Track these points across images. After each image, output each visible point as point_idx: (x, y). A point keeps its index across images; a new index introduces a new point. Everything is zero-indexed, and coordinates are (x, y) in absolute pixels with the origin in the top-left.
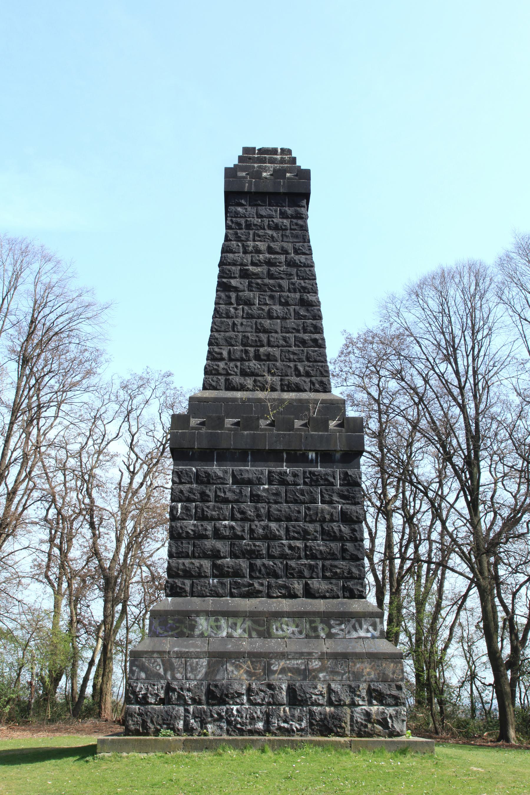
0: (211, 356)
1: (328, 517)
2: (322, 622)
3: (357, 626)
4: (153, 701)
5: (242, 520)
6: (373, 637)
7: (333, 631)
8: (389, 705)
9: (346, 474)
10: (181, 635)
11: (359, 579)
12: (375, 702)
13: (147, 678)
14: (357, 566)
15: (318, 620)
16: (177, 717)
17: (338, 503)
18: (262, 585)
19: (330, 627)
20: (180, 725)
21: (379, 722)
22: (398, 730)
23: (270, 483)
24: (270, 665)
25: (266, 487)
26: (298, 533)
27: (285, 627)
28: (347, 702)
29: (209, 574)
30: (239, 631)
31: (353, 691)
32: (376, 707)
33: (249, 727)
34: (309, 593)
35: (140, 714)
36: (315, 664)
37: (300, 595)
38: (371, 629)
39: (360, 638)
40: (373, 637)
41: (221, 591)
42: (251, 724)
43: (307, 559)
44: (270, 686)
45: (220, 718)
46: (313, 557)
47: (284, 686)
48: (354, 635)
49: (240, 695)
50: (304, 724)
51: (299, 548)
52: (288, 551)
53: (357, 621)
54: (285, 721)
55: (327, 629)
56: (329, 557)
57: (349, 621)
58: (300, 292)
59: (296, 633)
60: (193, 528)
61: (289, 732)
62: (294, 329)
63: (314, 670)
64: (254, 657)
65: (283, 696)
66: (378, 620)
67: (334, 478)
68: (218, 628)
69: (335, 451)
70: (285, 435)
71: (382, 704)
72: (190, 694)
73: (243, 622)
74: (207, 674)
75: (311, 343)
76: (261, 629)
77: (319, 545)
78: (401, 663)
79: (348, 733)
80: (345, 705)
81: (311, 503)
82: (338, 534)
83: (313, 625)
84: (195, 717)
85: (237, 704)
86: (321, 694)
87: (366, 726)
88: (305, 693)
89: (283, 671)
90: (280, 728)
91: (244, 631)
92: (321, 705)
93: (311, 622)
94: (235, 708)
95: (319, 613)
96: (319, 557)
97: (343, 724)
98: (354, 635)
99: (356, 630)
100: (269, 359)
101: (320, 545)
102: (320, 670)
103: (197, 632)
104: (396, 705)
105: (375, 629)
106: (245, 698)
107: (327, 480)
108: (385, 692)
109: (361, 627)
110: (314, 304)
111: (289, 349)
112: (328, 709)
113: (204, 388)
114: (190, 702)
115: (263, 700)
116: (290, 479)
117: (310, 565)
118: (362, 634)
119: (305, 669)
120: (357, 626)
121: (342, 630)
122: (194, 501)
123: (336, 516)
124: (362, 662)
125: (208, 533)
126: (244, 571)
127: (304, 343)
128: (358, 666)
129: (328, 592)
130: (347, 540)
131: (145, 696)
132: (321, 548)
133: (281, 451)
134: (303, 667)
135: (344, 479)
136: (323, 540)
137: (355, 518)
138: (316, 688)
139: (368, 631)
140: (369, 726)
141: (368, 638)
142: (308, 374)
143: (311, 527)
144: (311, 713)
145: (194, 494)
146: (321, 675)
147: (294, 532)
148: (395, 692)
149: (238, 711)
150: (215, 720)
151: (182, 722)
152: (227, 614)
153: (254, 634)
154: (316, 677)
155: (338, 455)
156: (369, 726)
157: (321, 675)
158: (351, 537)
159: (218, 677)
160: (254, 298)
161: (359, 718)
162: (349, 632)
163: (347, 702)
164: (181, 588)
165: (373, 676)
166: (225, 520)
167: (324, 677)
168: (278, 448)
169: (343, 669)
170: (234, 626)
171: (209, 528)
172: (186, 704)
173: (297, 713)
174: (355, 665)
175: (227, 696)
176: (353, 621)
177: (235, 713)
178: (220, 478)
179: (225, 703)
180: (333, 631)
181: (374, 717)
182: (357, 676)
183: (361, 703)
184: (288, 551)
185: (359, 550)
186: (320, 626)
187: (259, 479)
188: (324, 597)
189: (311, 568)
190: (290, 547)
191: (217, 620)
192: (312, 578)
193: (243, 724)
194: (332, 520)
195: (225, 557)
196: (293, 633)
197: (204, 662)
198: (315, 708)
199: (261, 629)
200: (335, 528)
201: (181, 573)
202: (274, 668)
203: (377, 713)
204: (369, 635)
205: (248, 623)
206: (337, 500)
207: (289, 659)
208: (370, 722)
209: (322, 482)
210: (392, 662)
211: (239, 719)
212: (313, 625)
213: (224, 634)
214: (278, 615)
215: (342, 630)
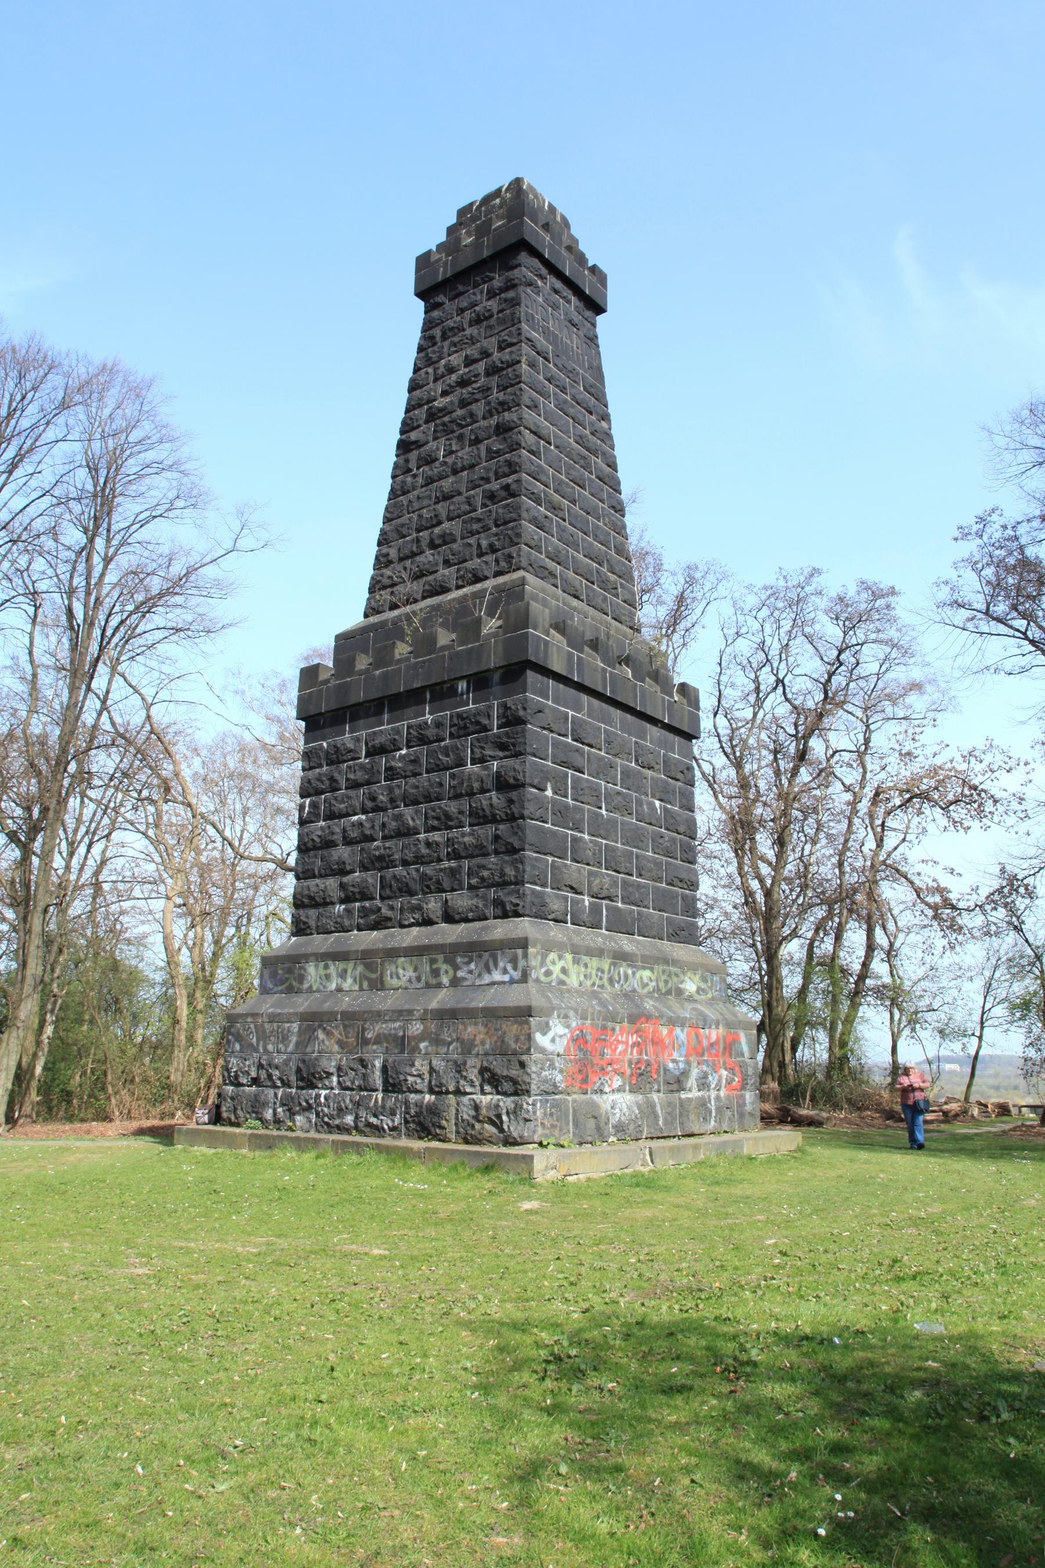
0: (382, 562)
1: (476, 785)
2: (446, 961)
3: (491, 964)
4: (245, 1081)
5: (373, 810)
6: (512, 981)
7: (460, 974)
8: (505, 1094)
9: (506, 708)
10: (290, 990)
11: (516, 884)
12: (488, 1088)
13: (241, 1051)
14: (514, 863)
15: (440, 957)
16: (265, 1104)
17: (494, 758)
18: (392, 908)
19: (456, 968)
20: (268, 1114)
21: (492, 1122)
22: (515, 1134)
23: (408, 747)
24: (364, 1030)
25: (404, 752)
26: (438, 819)
27: (401, 971)
28: (451, 1088)
29: (335, 900)
30: (349, 981)
31: (459, 1068)
32: (489, 1097)
33: (337, 1122)
34: (449, 918)
35: (232, 1098)
36: (416, 1028)
37: (435, 919)
38: (509, 967)
39: (493, 983)
40: (512, 981)
41: (347, 923)
42: (339, 1116)
43: (449, 860)
44: (363, 1063)
45: (309, 1108)
46: (455, 855)
47: (378, 1064)
48: (487, 979)
49: (329, 1075)
50: (397, 1120)
51: (437, 844)
52: (424, 851)
53: (491, 956)
54: (375, 1116)
55: (451, 972)
56: (477, 852)
57: (480, 956)
58: (499, 413)
59: (414, 980)
60: (319, 833)
61: (378, 1130)
62: (482, 478)
63: (414, 1038)
64: (348, 1019)
65: (377, 1078)
66: (520, 952)
67: (489, 717)
68: (328, 977)
69: (488, 670)
70: (424, 662)
71: (498, 1093)
72: (277, 1073)
73: (354, 968)
74: (297, 1044)
75: (503, 494)
76: (373, 976)
77: (463, 835)
78: (528, 1023)
79: (453, 1136)
80: (448, 1092)
81: (458, 766)
82: (488, 812)
83: (435, 966)
84: (283, 1105)
85: (326, 1088)
86: (419, 1076)
87: (473, 1127)
88: (398, 1073)
89: (378, 1040)
90: (369, 1125)
91: (355, 980)
92: (420, 1092)
93: (433, 961)
94: (323, 1093)
95: (443, 946)
96: (463, 854)
97: (444, 1123)
98: (487, 979)
99: (489, 972)
100: (445, 543)
101: (466, 835)
102: (421, 1038)
103: (306, 986)
104: (516, 1093)
105: (515, 968)
106: (335, 1079)
107: (478, 723)
108: (499, 1072)
109: (496, 966)
110: (513, 425)
111: (473, 515)
112: (427, 1097)
113: (366, 616)
114: (279, 1083)
115: (353, 1083)
116: (431, 733)
117: (451, 869)
118: (497, 976)
119: (403, 1037)
120: (491, 964)
121: (471, 972)
122: (322, 792)
123: (489, 783)
124: (476, 1024)
125: (335, 837)
126: (372, 889)
127: (491, 497)
128: (469, 1030)
129: (471, 910)
130: (502, 820)
131: (236, 1077)
132: (466, 839)
133: (422, 689)
134: (401, 1034)
135: (504, 716)
136: (471, 825)
137: (512, 781)
138: (413, 1065)
139: (505, 971)
140: (478, 1126)
141: (504, 983)
142: (493, 549)
143: (452, 807)
144: (407, 1103)
145: (322, 782)
146: (422, 1045)
147: (434, 818)
148: (514, 1073)
149: (326, 1098)
150: (305, 1110)
151: (271, 1111)
152: (339, 956)
153: (365, 984)
154: (415, 1049)
155: (496, 677)
156: (478, 1126)
157: (422, 1045)
158: (507, 814)
159: (309, 1049)
160: (438, 449)
161: (467, 1114)
162: (480, 975)
163: (451, 1088)
164: (305, 923)
165: (487, 1046)
166: (355, 814)
167: (426, 1048)
168: (415, 686)
169: (450, 1036)
170: (343, 975)
171: (337, 830)
172: (275, 1087)
173: (391, 1102)
174: (466, 1029)
175: (313, 1074)
176: (486, 955)
177: (322, 1100)
178: (351, 751)
179: (313, 1086)
180: (460, 974)
181: (484, 1112)
182: (467, 1047)
183: (468, 1089)
184: (424, 851)
185: (516, 834)
186: (444, 967)
187: (394, 741)
188: (467, 920)
189: (453, 873)
190: (428, 844)
191: (326, 967)
192: (453, 890)
193: (331, 1117)
194: (483, 791)
195: (353, 871)
196: (410, 981)
197: (295, 1027)
198: (412, 1096)
199: (373, 976)
200: (484, 802)
201: (306, 901)
202: (369, 1035)
203: (489, 1107)
204: (506, 978)
205: (360, 968)
206: (491, 753)
207: (386, 1021)
208: (479, 1121)
209: (472, 728)
210: (516, 1022)
211: (326, 1110)
212: (435, 966)
213: (333, 986)
214: (392, 954)
215: (471, 972)
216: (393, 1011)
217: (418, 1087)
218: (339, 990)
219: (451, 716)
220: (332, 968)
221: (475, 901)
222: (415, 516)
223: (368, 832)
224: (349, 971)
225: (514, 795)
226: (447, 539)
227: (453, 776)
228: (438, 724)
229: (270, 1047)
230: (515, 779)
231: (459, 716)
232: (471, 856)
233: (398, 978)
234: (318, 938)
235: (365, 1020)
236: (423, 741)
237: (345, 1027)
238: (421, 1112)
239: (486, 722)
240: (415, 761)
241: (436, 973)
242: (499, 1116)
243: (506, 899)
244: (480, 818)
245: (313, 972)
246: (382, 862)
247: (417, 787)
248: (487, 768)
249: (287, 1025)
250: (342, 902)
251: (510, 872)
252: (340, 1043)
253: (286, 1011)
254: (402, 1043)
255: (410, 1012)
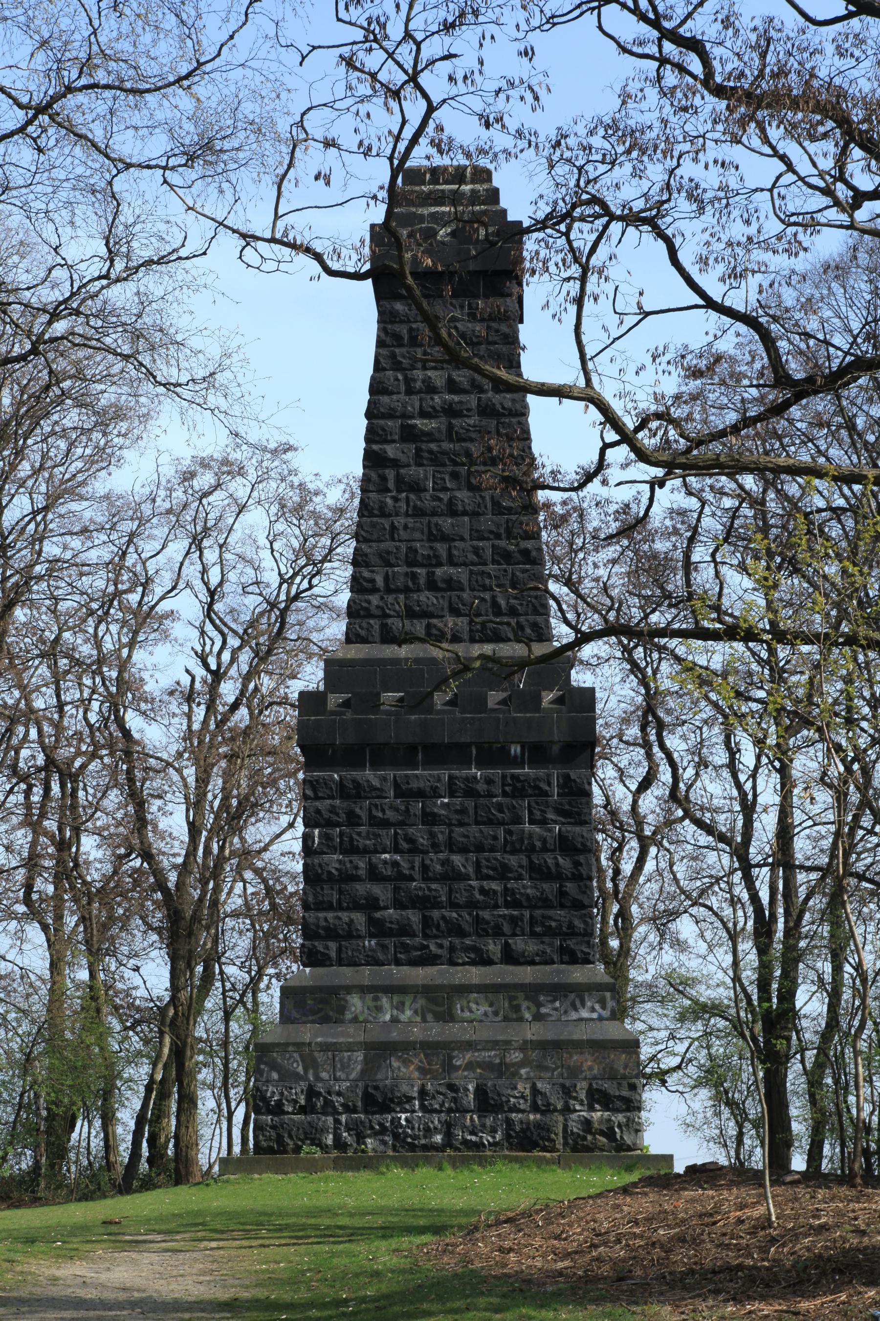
1: (538, 844)
3: (578, 1003)
5: (410, 851)
6: (601, 1019)
7: (543, 1010)
9: (567, 777)
10: (325, 1020)
12: (597, 1106)
13: (280, 1079)
14: (582, 917)
15: (521, 995)
17: (555, 822)
18: (441, 946)
19: (539, 1005)
21: (602, 1133)
22: (629, 1142)
23: (451, 795)
24: (451, 1058)
28: (559, 1107)
31: (567, 1092)
34: (510, 957)
38: (597, 1007)
41: (381, 956)
45: (384, 1130)
46: (516, 904)
48: (574, 1016)
50: (498, 1137)
55: (534, 1009)
62: (491, 532)
63: (513, 1065)
67: (549, 784)
68: (379, 1009)
77: (525, 887)
82: (553, 870)
86: (523, 1097)
89: (470, 1066)
90: (465, 1142)
91: (416, 1012)
93: (511, 999)
98: (574, 1016)
99: (576, 1010)
101: (527, 887)
102: (522, 1064)
103: (348, 1016)
104: (628, 1110)
105: (604, 1007)
107: (537, 787)
109: (583, 1005)
114: (340, 1109)
116: (481, 787)
118: (585, 1014)
119: (501, 1064)
120: (578, 1003)
121: (556, 1009)
127: (507, 557)
130: (567, 878)
132: (529, 891)
138: (515, 1088)
139: (593, 1010)
140: (589, 1137)
142: (513, 612)
143: (513, 861)
144: (509, 1122)
145: (337, 815)
147: (488, 867)
148: (625, 1093)
152: (389, 990)
153: (429, 1017)
154: (515, 1074)
156: (589, 1137)
157: (523, 1071)
160: (426, 479)
162: (566, 1012)
166: (385, 852)
168: (463, 740)
170: (400, 1007)
176: (572, 996)
179: (390, 1110)
180: (543, 1010)
185: (584, 893)
186: (525, 1005)
187: (435, 789)
188: (532, 963)
190: (482, 891)
191: (376, 999)
193: (414, 1137)
195: (386, 908)
197: (359, 1056)
200: (549, 861)
204: (595, 1015)
208: (591, 1133)
213: (388, 1017)
214: (464, 990)
215: (556, 1009)
216: (487, 1042)
217: (522, 1107)
218: (395, 1020)
219: (504, 777)
220: (384, 1000)
221: (541, 947)
222: (403, 547)
223: (407, 872)
224: (407, 1004)
225: (582, 858)
226: (451, 584)
227: (510, 832)
228: (489, 781)
229: (324, 1075)
230: (583, 844)
231: (513, 776)
232: (532, 907)
233: (471, 1011)
234: (367, 970)
235: (453, 1049)
236: (471, 793)
237: (426, 1056)
238: (528, 1128)
239: (546, 788)
240: (463, 811)
241: (517, 1009)
242: (611, 1129)
243: (576, 948)
244: (539, 873)
245: (356, 1004)
246: (424, 903)
247: (467, 837)
248: (550, 830)
249: (346, 1054)
250: (372, 936)
251: (578, 923)
252: (420, 1069)
253: (341, 1040)
254: (502, 1069)
255: (508, 1042)
